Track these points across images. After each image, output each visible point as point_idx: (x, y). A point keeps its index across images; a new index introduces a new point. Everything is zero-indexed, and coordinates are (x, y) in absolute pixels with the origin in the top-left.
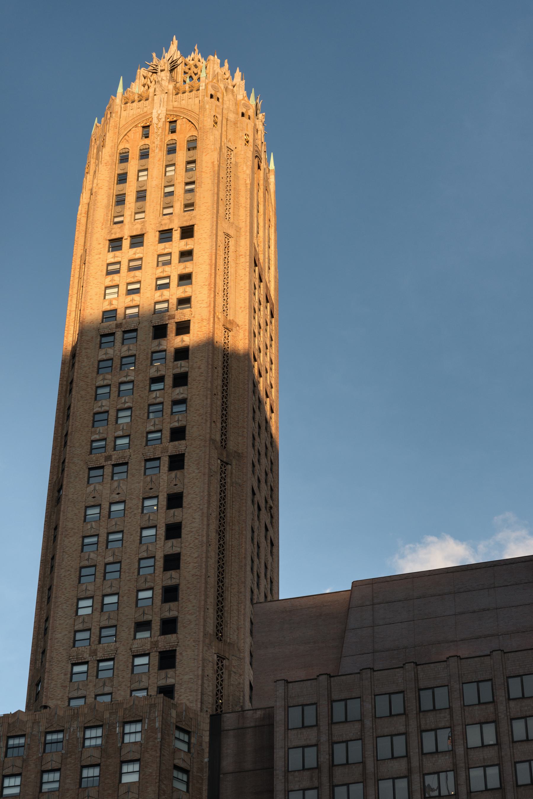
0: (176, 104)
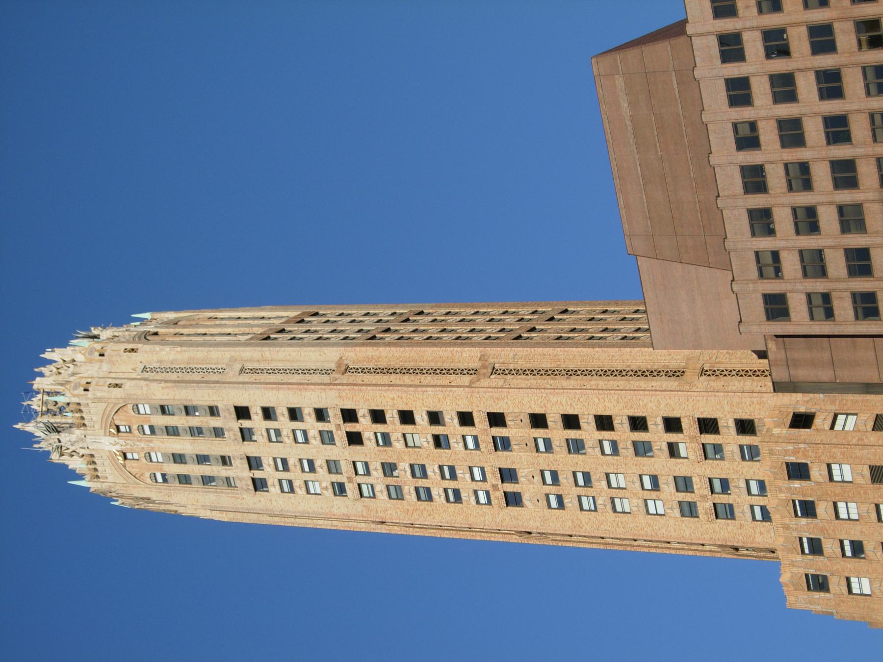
0: (97, 426)
